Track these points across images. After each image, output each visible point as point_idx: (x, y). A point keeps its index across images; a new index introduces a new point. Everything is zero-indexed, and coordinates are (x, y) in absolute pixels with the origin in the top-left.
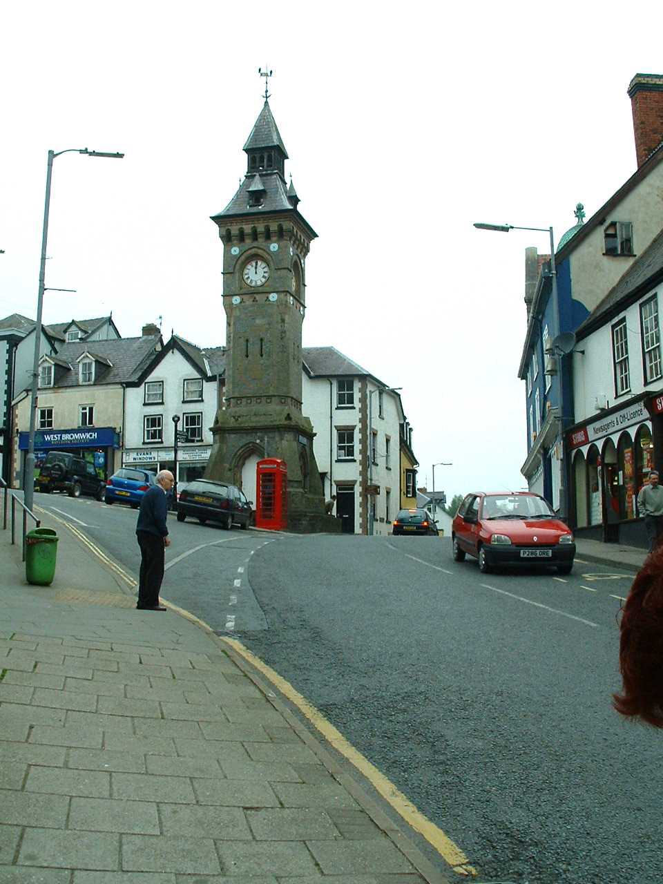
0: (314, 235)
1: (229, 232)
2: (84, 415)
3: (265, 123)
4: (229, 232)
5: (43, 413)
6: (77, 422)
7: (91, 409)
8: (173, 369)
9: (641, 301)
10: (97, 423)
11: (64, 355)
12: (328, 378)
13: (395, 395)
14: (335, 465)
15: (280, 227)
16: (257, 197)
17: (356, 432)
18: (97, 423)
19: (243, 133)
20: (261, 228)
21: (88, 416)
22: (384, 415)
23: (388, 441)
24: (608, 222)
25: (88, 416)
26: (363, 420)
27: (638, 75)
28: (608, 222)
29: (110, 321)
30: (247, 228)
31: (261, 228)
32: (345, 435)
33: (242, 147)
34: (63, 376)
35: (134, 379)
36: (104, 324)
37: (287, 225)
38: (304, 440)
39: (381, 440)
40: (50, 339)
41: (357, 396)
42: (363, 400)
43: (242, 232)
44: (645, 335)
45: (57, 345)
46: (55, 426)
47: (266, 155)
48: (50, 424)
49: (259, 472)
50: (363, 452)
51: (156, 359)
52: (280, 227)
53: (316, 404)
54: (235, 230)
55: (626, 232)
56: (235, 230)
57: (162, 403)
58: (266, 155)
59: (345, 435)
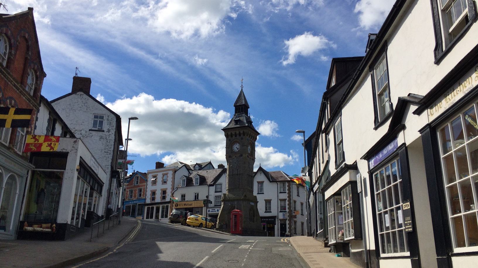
1: (228, 134)
2: (196, 196)
3: (241, 95)
4: (228, 134)
7: (198, 194)
9: (451, 120)
15: (244, 132)
17: (287, 201)
20: (238, 132)
22: (300, 195)
23: (302, 204)
26: (289, 197)
30: (233, 133)
31: (238, 132)
33: (400, 96)
35: (212, 183)
38: (252, 204)
42: (289, 190)
43: (231, 133)
44: (375, 193)
48: (184, 199)
50: (289, 208)
52: (244, 132)
55: (82, 199)
56: (229, 133)
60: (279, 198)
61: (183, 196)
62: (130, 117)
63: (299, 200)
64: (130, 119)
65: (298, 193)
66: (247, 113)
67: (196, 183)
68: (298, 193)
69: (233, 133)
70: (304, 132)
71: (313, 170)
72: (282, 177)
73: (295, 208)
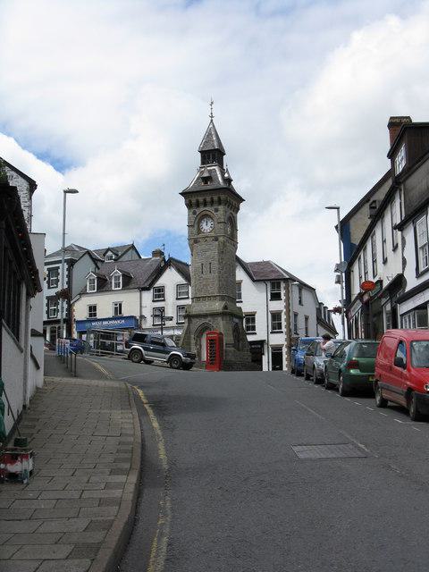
0: (242, 200)
1: (190, 201)
2: (116, 308)
3: (212, 134)
4: (190, 201)
5: (280, 327)
6: (111, 314)
7: (120, 305)
8: (170, 279)
10: (125, 313)
11: (103, 271)
12: (264, 281)
13: (312, 290)
14: (271, 335)
15: (219, 198)
16: (206, 180)
17: (283, 314)
18: (125, 313)
19: (197, 142)
21: (118, 308)
23: (307, 319)
24: (371, 201)
25: (118, 308)
26: (288, 307)
27: (391, 118)
28: (371, 201)
29: (133, 247)
30: (201, 199)
32: (276, 316)
34: (103, 285)
35: (147, 285)
36: (128, 250)
37: (223, 197)
38: (237, 320)
39: (301, 320)
40: (95, 260)
41: (283, 292)
43: (198, 201)
45: (99, 264)
46: (98, 317)
47: (212, 154)
48: (95, 315)
49: (208, 339)
51: (159, 272)
52: (219, 198)
53: (253, 299)
54: (194, 200)
56: (194, 200)
57: (164, 300)
58: (212, 154)
59: (276, 316)
60: (270, 309)
61: (93, 309)
62: (66, 189)
63: (302, 312)
64: (65, 192)
65: (300, 298)
66: (221, 164)
67: (117, 285)
68: (300, 298)
69: (201, 199)
70: (338, 208)
71: (356, 268)
72: (272, 271)
73: (296, 325)
